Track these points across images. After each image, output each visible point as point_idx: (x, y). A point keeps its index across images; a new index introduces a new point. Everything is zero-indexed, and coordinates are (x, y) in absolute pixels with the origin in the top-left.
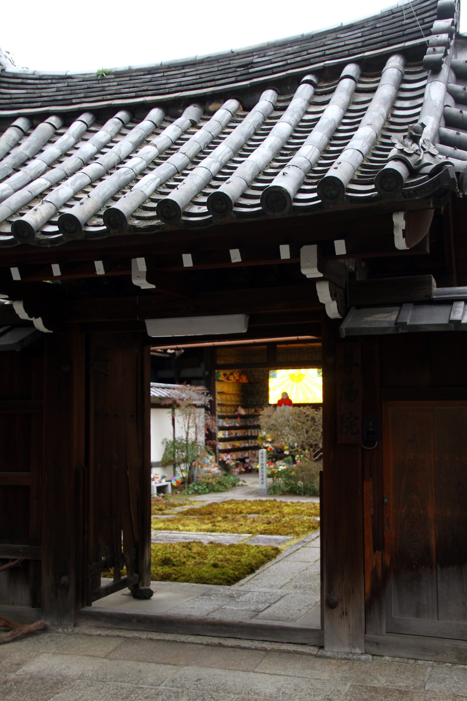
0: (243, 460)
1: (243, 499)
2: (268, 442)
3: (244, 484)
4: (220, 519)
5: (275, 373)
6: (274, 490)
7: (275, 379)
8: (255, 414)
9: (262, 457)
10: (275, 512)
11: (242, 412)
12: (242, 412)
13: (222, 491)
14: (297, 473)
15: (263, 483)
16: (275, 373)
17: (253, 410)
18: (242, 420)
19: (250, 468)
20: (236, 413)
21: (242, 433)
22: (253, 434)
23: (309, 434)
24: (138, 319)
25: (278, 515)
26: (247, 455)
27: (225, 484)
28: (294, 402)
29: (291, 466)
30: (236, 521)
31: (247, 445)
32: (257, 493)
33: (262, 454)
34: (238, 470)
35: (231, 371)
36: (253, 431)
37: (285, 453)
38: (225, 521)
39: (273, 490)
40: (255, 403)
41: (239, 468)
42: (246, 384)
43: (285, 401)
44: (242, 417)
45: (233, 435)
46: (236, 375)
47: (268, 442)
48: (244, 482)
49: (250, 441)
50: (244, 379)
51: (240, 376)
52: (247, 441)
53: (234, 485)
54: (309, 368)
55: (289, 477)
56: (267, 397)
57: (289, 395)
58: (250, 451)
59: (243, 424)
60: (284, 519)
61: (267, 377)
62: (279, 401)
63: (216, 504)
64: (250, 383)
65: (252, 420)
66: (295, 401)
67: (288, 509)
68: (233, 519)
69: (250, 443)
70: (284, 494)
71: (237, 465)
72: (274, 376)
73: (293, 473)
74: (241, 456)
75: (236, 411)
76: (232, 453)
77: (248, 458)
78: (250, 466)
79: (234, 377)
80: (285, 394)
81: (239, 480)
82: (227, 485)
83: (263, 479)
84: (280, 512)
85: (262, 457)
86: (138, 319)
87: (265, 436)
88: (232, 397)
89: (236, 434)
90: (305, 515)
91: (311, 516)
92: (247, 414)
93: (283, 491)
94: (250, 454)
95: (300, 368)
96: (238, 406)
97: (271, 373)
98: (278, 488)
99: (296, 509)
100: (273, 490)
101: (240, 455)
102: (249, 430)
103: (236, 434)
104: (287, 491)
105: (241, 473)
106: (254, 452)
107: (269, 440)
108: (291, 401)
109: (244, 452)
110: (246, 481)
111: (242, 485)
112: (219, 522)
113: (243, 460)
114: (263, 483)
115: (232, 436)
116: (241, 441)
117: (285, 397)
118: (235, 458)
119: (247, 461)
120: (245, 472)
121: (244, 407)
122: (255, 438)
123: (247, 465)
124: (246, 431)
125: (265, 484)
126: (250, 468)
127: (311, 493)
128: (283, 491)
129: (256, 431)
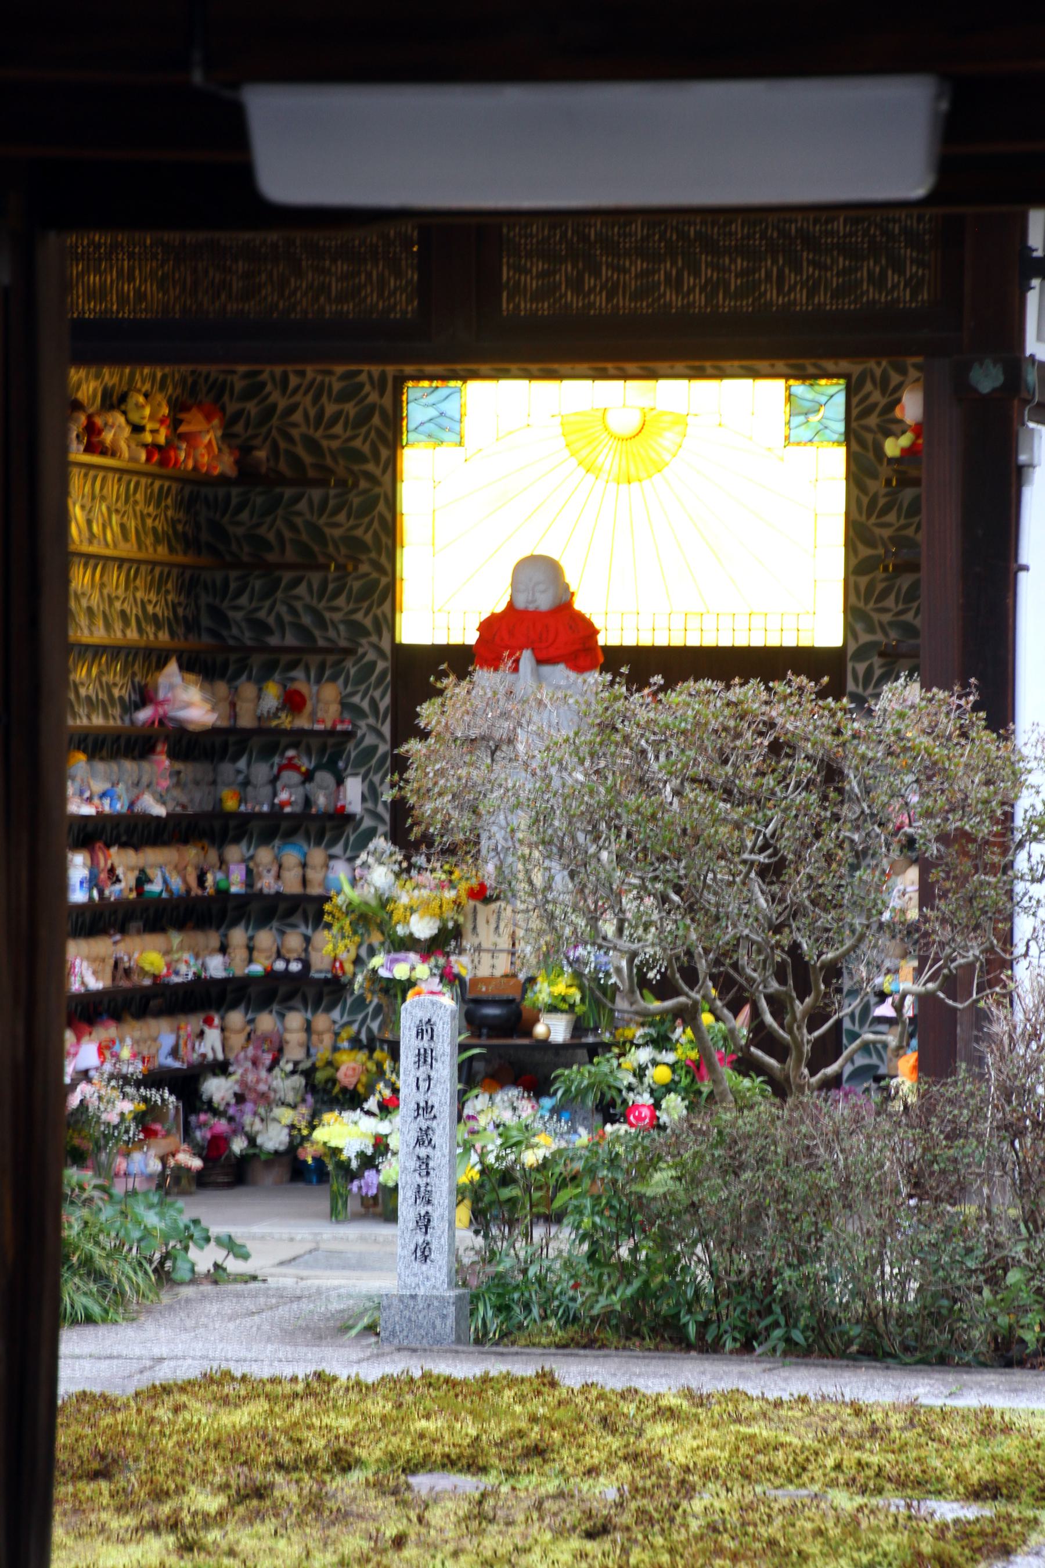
0: (186, 1083)
1: (303, 1370)
2: (408, 944)
3: (233, 1266)
4: (212, 1503)
5: (450, 407)
6: (503, 1309)
7: (448, 452)
8: (286, 721)
9: (424, 1057)
10: (598, 1458)
11: (193, 704)
12: (193, 704)
13: (89, 1319)
14: (689, 1178)
15: (423, 1253)
16: (450, 407)
17: (272, 695)
18: (189, 770)
19: (238, 1145)
20: (144, 715)
21: (181, 872)
22: (267, 884)
23: (797, 891)
24: (197, 77)
25: (366, 1545)
26: (211, 1044)
27: (101, 1263)
28: (613, 633)
29: (583, 1137)
30: (343, 1516)
31: (216, 967)
32: (371, 1329)
33: (426, 1029)
34: (146, 1162)
35: (111, 377)
36: (264, 855)
37: (540, 1030)
38: (258, 1515)
39: (497, 1310)
40: (290, 640)
41: (161, 1145)
42: (223, 480)
43: (543, 629)
44: (189, 745)
45: (121, 889)
46: (149, 411)
47: (408, 944)
48: (231, 1245)
49: (238, 936)
50: (207, 449)
51: (179, 408)
52: (214, 939)
53: (164, 1276)
54: (721, 374)
55: (631, 1215)
56: (382, 591)
57: (571, 578)
58: (236, 1018)
59: (197, 801)
60: (697, 1505)
61: (385, 434)
62: (489, 626)
63: (108, 1403)
64: (247, 473)
65: (261, 772)
66: (621, 621)
67: (691, 1443)
68: (315, 1505)
69: (239, 954)
70: (587, 1335)
71: (147, 1122)
72: (446, 428)
73: (661, 1181)
74: (174, 1052)
75: (145, 696)
76: (108, 1031)
77: (221, 1068)
78: (238, 1129)
79: (137, 429)
80: (541, 569)
81: (192, 1235)
82: (120, 1271)
83: (425, 1223)
84: (633, 1458)
85: (424, 1057)
86: (197, 77)
87: (385, 902)
88: (115, 578)
89: (143, 879)
90: (833, 1484)
91: (879, 1491)
92: (224, 723)
93: (570, 1319)
94: (237, 1040)
95: (652, 375)
96: (156, 659)
97: (421, 402)
98: (535, 1296)
99: (750, 1439)
100: (497, 1310)
101: (162, 1040)
102: (234, 853)
103: (143, 879)
104: (605, 1319)
105: (172, 1183)
106: (266, 1022)
107: (423, 928)
108: (587, 630)
109: (193, 1023)
110: (251, 1246)
111: (218, 1275)
112: (208, 1521)
113: (186, 1083)
114: (423, 1253)
115: (113, 892)
116: (176, 939)
117: (544, 602)
118: (136, 1069)
119: (217, 1089)
120: (202, 1181)
121: (202, 666)
122: (308, 909)
123: (222, 1125)
124: (213, 855)
125: (440, 1257)
126: (238, 1145)
127: (797, 1336)
128: (570, 1319)
129: (291, 857)
